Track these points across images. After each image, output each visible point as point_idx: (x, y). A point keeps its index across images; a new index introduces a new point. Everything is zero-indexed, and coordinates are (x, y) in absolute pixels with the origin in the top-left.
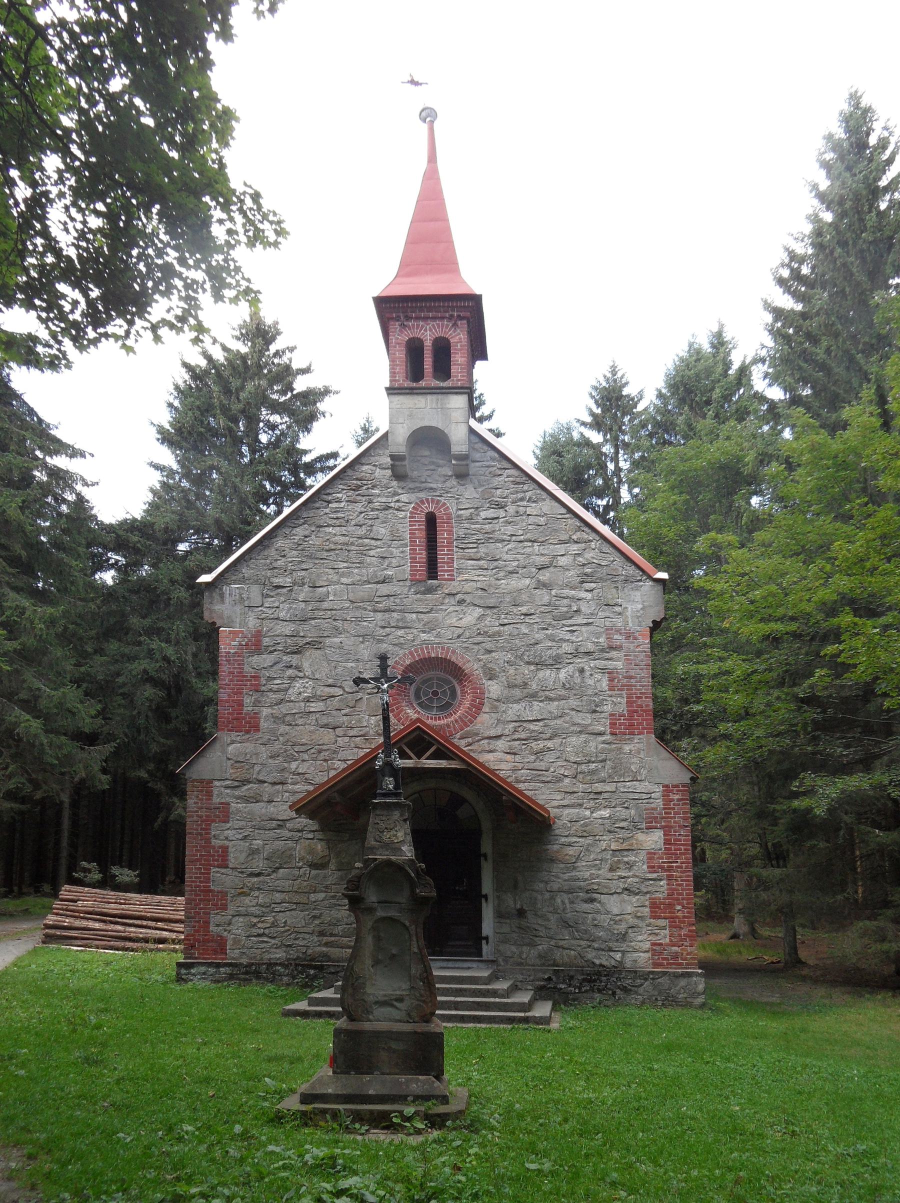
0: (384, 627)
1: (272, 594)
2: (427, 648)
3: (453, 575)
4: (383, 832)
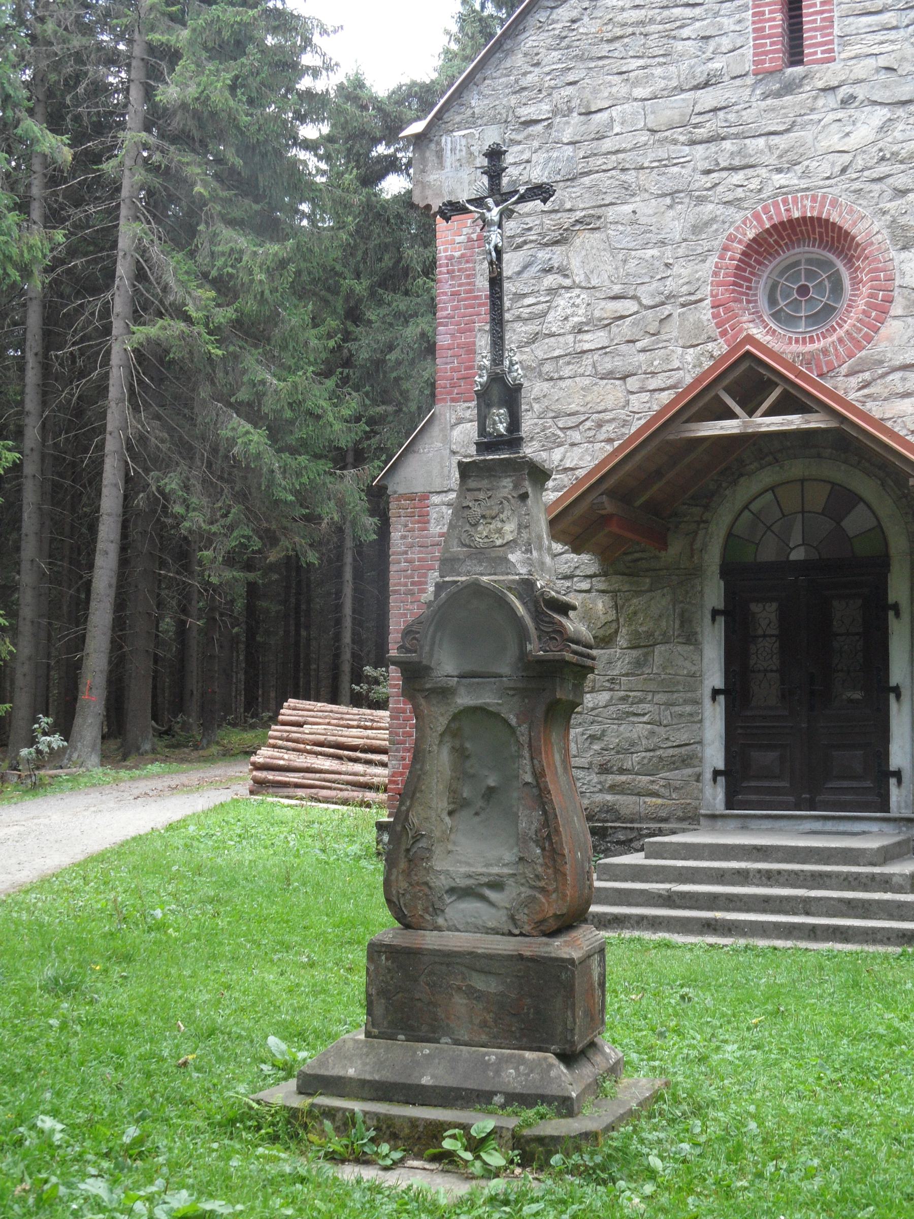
0: (708, 172)
1: (519, 137)
2: (785, 202)
3: (832, 51)
4: (475, 525)
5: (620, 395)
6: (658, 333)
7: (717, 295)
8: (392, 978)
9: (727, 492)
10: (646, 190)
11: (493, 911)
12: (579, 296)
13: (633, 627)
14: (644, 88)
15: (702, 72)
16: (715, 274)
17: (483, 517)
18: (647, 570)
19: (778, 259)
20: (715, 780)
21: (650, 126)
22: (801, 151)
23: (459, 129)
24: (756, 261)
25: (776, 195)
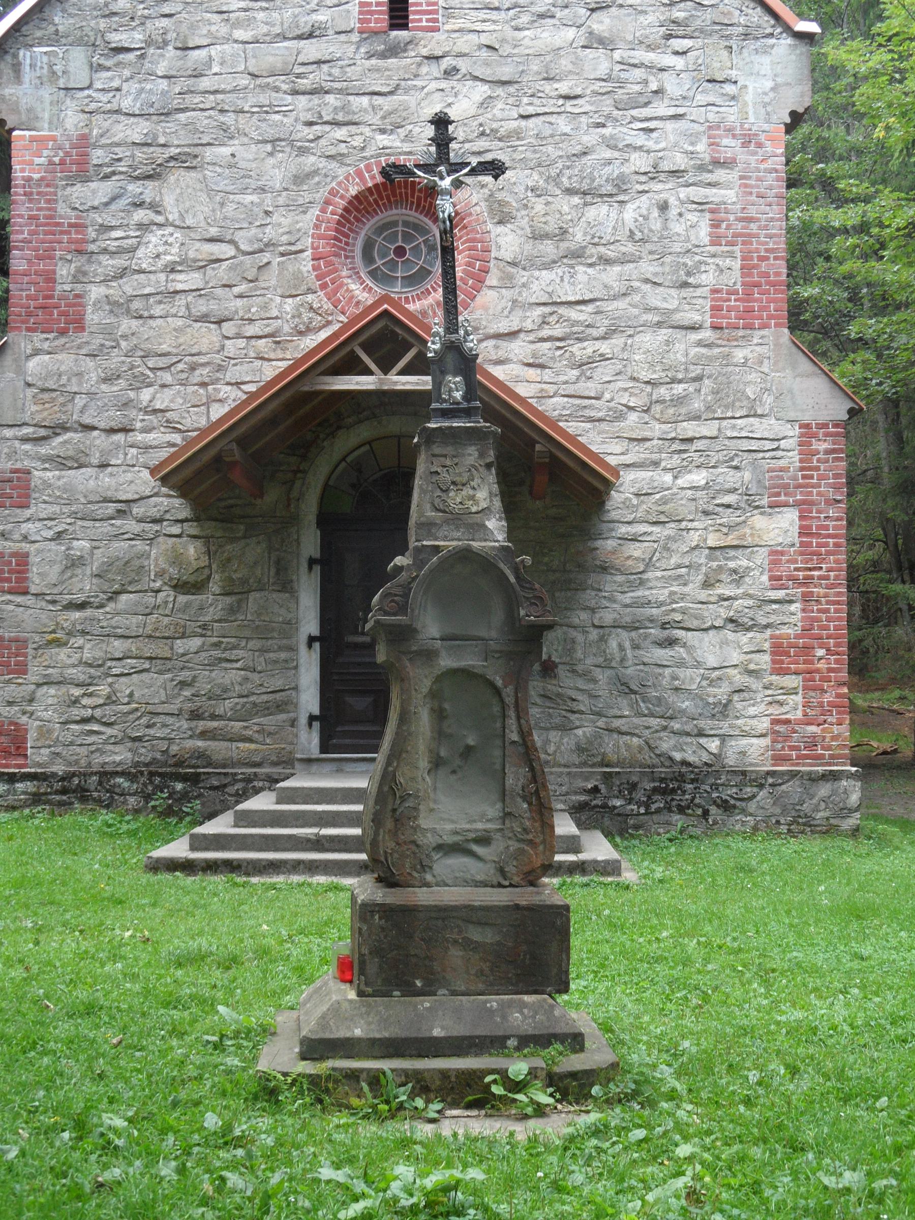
0: (310, 124)
1: (109, 63)
3: (436, 20)
4: (446, 491)
5: (215, 339)
6: (256, 280)
7: (318, 247)
8: (385, 937)
9: (325, 443)
10: (245, 135)
11: (480, 865)
12: (172, 235)
13: (227, 574)
14: (246, 30)
15: (306, 23)
16: (317, 227)
17: (454, 483)
18: (243, 517)
19: (377, 218)
20: (310, 725)
21: (251, 69)
22: (404, 114)
23: (40, 45)
24: (355, 217)
25: (380, 155)
